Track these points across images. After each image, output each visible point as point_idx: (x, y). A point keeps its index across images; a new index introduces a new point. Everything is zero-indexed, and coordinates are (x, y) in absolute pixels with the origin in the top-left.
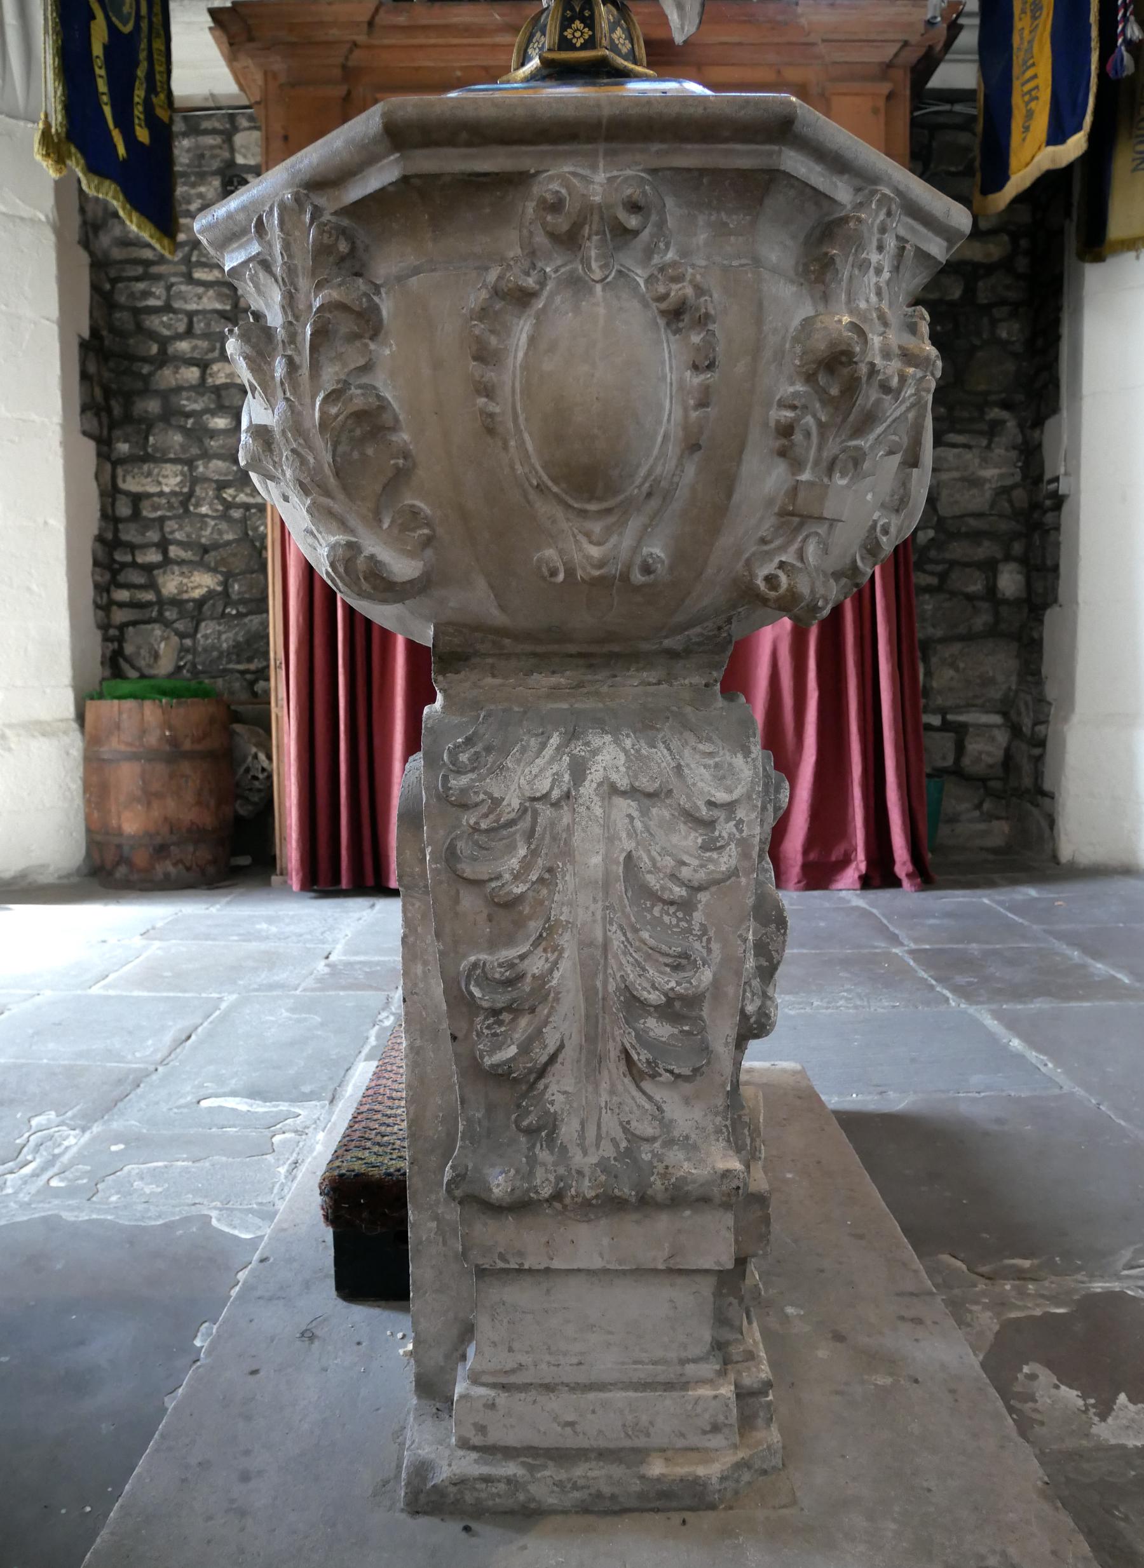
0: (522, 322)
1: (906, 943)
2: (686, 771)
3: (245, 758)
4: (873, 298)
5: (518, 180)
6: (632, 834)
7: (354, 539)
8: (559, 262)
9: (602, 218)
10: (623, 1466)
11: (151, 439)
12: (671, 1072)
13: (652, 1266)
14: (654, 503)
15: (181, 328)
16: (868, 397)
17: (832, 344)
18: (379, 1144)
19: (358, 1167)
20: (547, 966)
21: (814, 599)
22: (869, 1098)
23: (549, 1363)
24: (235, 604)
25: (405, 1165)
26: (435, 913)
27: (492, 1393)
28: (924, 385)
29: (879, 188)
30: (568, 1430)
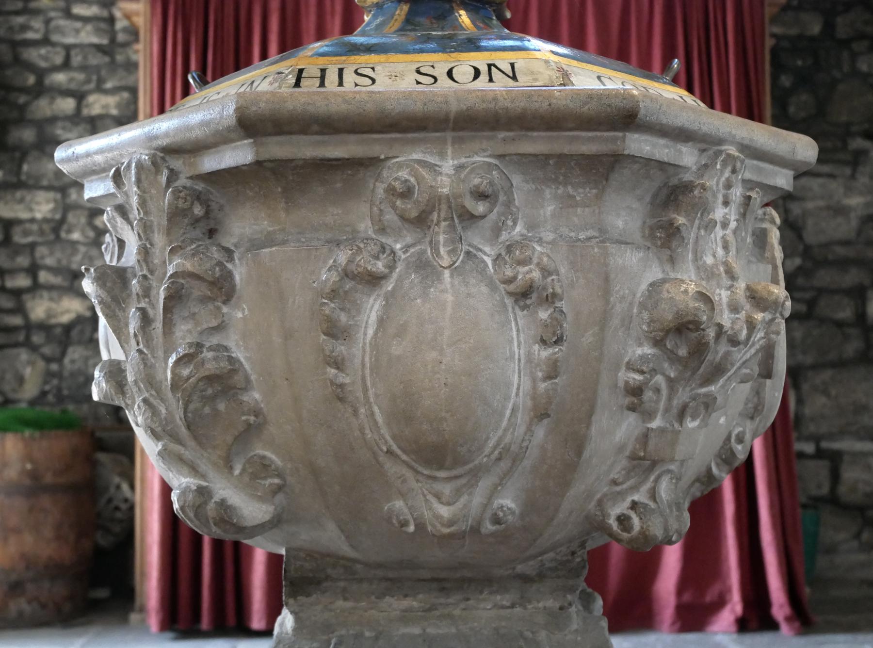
0: (371, 300)
3: (107, 489)
4: (720, 252)
5: (371, 163)
7: (204, 484)
8: (409, 240)
9: (450, 207)
11: (25, 167)
14: (504, 465)
15: (59, 60)
16: (717, 352)
17: (678, 314)
28: (774, 328)
29: (723, 148)
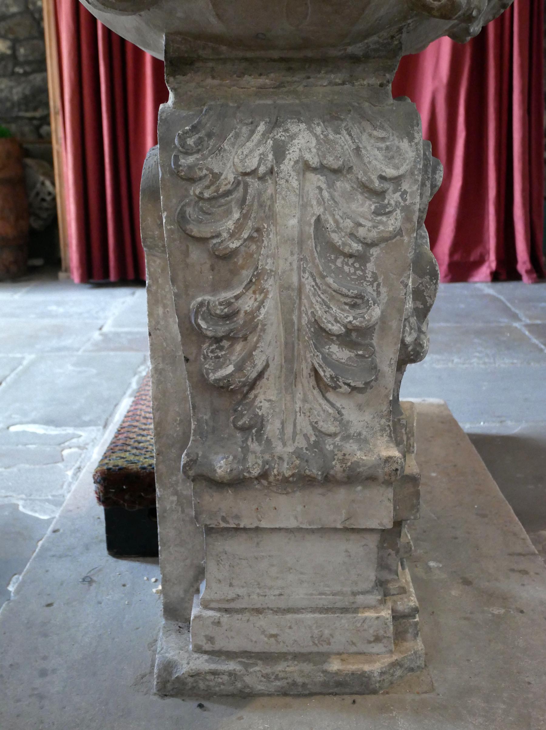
1: (523, 319)
2: (363, 152)
3: (34, 186)
6: (321, 201)
10: (312, 664)
12: (349, 385)
13: (333, 526)
18: (137, 448)
19: (121, 463)
20: (256, 304)
21: (470, 9)
22: (493, 425)
23: (258, 595)
24: (21, 64)
25: (154, 461)
26: (170, 264)
27: (218, 614)
30: (273, 640)
